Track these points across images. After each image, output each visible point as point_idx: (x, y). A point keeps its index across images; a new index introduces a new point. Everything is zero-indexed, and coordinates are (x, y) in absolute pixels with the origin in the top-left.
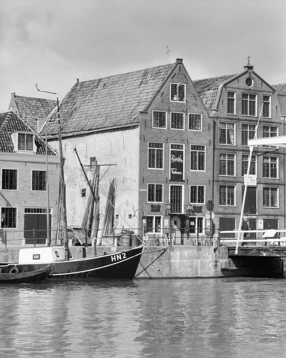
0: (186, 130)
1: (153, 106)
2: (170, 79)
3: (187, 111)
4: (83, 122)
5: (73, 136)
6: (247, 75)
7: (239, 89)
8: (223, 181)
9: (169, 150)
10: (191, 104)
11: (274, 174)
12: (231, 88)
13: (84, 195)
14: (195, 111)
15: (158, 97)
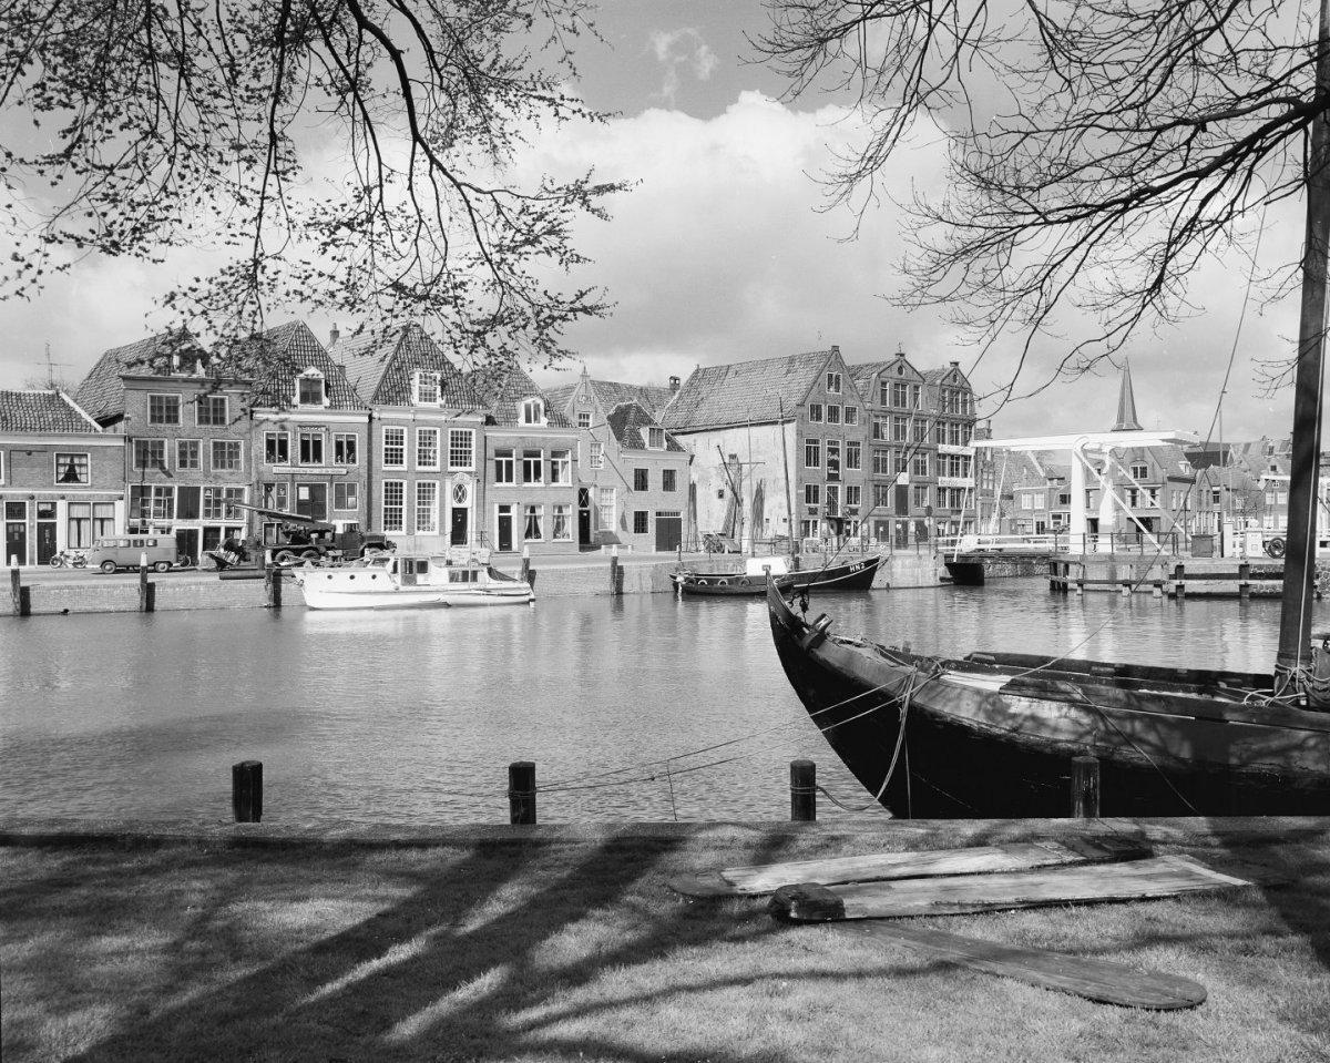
1: (811, 397)
4: (717, 415)
5: (706, 430)
6: (899, 364)
11: (924, 473)
13: (721, 496)
14: (851, 403)
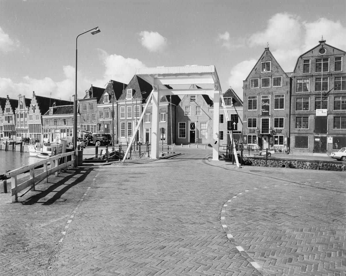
0: (272, 87)
3: (260, 77)
6: (321, 47)
7: (312, 57)
9: (260, 99)
10: (274, 72)
14: (277, 75)
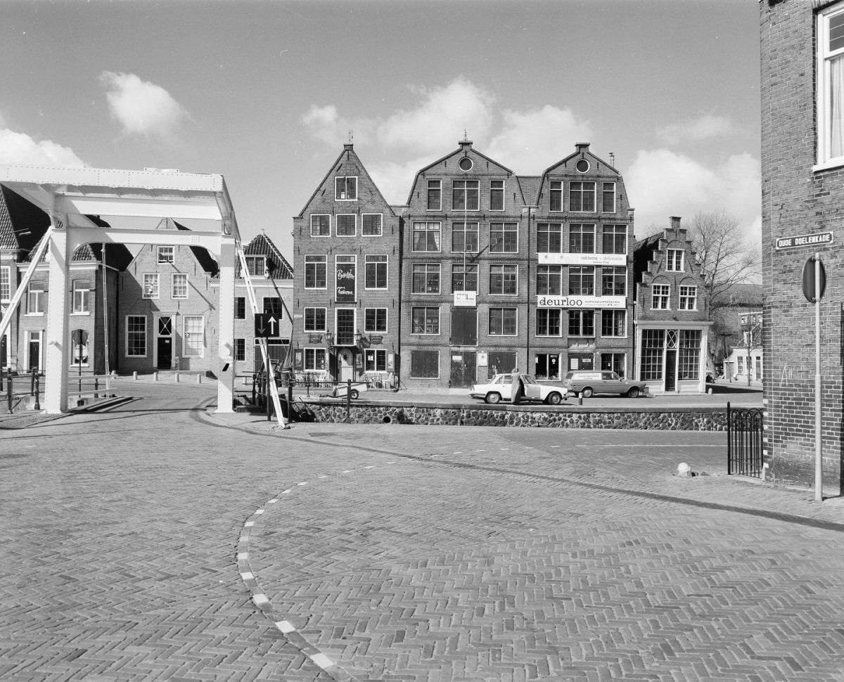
0: (359, 236)
1: (311, 208)
2: (334, 172)
6: (579, 157)
7: (446, 174)
8: (418, 301)
12: (431, 175)
14: (370, 210)
15: (318, 196)
